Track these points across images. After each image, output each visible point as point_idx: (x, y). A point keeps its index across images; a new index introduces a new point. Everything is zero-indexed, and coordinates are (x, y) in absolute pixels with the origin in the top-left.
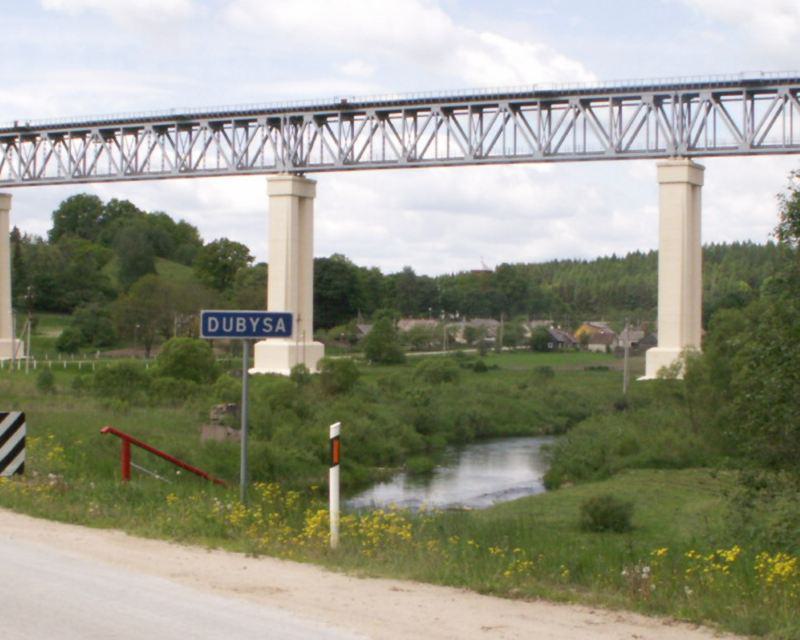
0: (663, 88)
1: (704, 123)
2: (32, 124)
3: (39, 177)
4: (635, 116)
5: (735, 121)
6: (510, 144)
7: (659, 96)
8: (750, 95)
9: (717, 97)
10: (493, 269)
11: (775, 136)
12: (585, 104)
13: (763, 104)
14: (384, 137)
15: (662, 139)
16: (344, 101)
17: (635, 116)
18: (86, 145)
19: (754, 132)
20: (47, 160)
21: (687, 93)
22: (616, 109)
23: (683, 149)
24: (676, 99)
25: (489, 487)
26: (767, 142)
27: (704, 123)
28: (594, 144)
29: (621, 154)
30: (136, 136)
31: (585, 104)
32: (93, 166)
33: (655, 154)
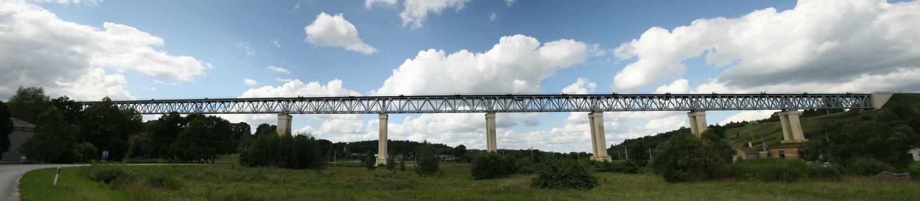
13: (353, 102)
20: (291, 106)
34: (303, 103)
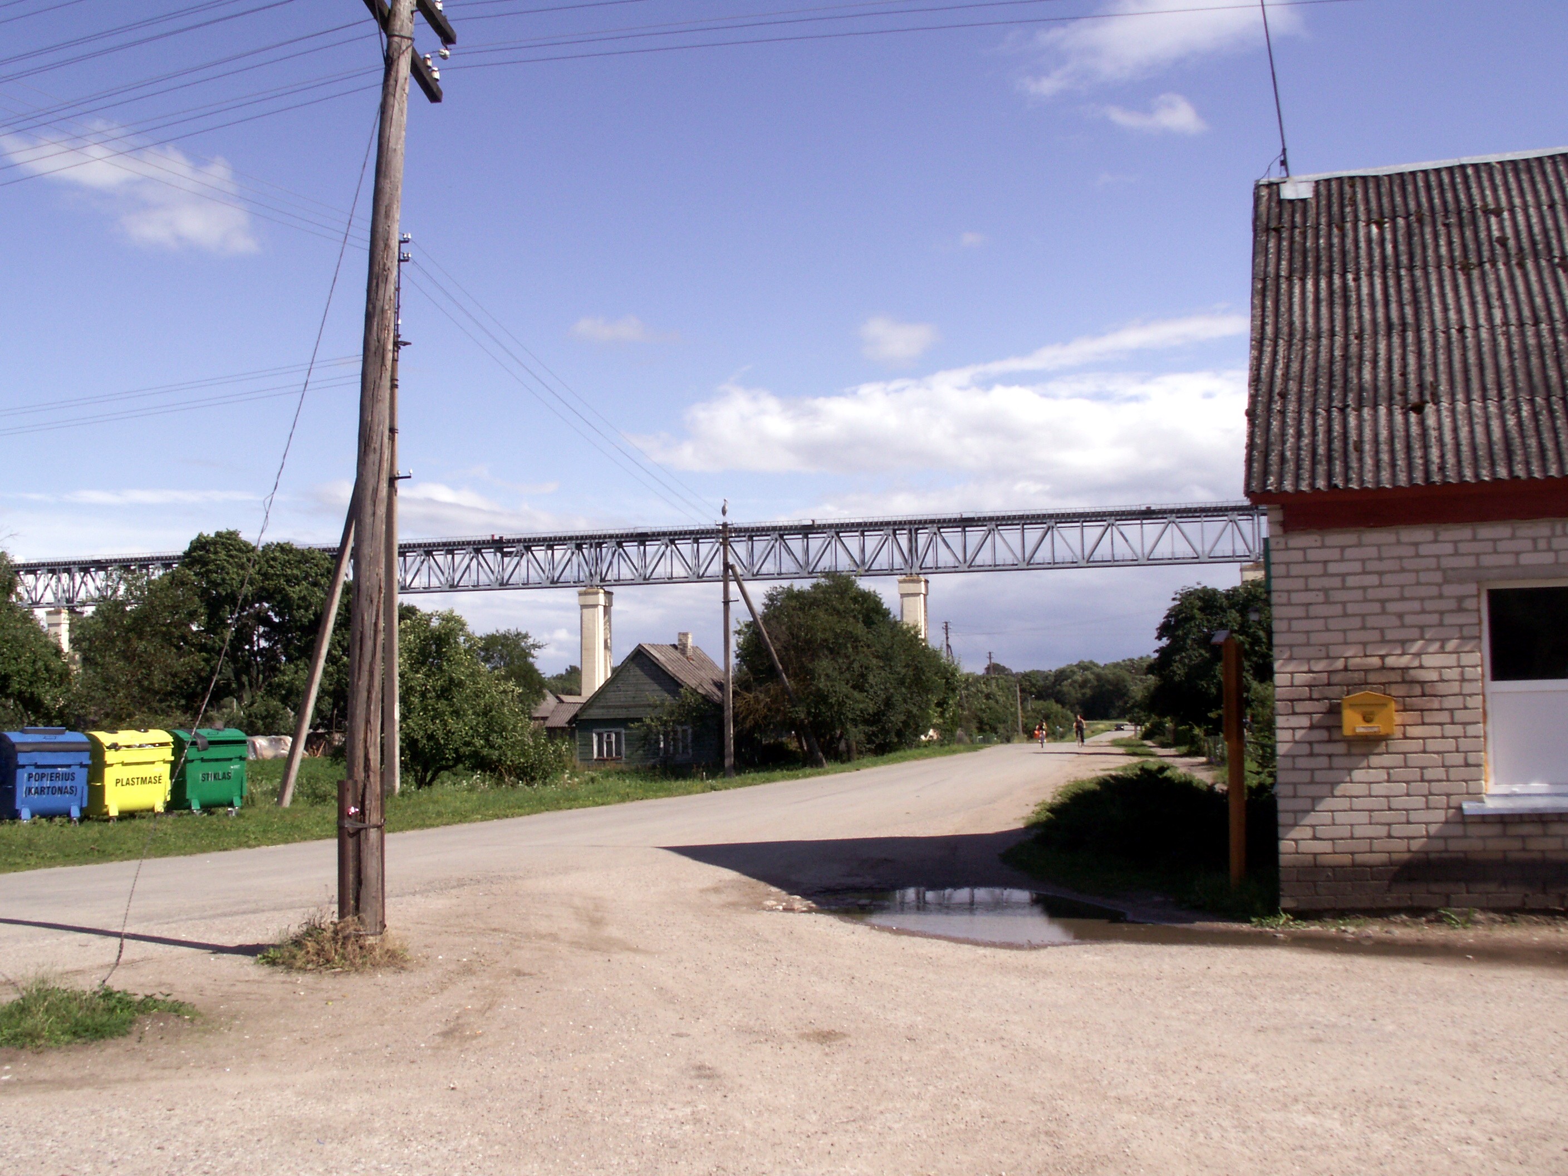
0: (582, 538)
1: (611, 563)
2: (817, 522)
3: (457, 586)
4: (563, 556)
5: (1050, 546)
6: (474, 577)
7: (579, 542)
8: (696, 541)
9: (620, 545)
10: (564, 672)
11: (662, 571)
12: (528, 549)
13: (652, 548)
14: (479, 563)
15: (582, 574)
16: (1149, 508)
17: (563, 556)
18: (37, 579)
19: (753, 564)
21: (597, 541)
22: (642, 548)
23: (597, 580)
24: (591, 546)
25: (1420, 936)
26: (708, 573)
27: (611, 563)
28: (679, 571)
29: (555, 583)
30: (36, 575)
31: (528, 549)
32: (42, 597)
33: (992, 568)
34: (558, 554)
